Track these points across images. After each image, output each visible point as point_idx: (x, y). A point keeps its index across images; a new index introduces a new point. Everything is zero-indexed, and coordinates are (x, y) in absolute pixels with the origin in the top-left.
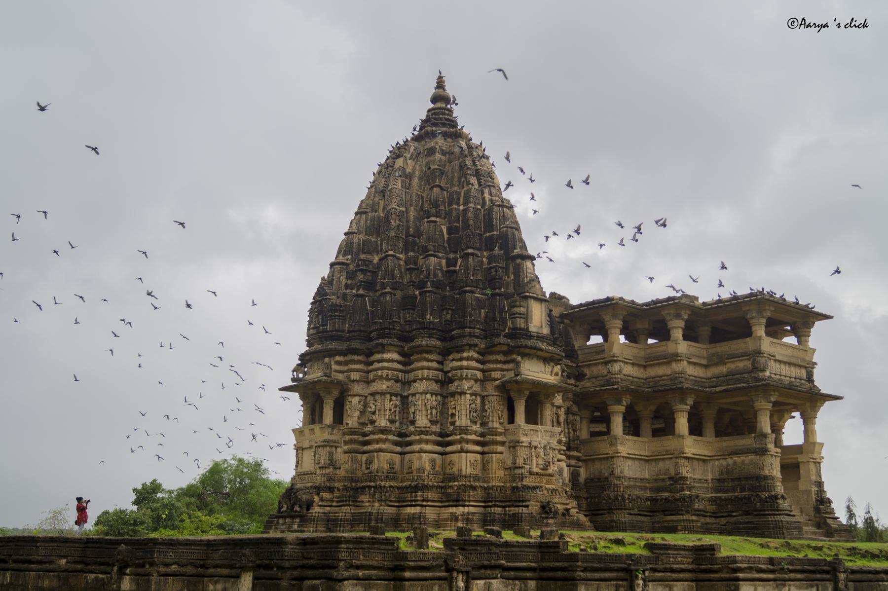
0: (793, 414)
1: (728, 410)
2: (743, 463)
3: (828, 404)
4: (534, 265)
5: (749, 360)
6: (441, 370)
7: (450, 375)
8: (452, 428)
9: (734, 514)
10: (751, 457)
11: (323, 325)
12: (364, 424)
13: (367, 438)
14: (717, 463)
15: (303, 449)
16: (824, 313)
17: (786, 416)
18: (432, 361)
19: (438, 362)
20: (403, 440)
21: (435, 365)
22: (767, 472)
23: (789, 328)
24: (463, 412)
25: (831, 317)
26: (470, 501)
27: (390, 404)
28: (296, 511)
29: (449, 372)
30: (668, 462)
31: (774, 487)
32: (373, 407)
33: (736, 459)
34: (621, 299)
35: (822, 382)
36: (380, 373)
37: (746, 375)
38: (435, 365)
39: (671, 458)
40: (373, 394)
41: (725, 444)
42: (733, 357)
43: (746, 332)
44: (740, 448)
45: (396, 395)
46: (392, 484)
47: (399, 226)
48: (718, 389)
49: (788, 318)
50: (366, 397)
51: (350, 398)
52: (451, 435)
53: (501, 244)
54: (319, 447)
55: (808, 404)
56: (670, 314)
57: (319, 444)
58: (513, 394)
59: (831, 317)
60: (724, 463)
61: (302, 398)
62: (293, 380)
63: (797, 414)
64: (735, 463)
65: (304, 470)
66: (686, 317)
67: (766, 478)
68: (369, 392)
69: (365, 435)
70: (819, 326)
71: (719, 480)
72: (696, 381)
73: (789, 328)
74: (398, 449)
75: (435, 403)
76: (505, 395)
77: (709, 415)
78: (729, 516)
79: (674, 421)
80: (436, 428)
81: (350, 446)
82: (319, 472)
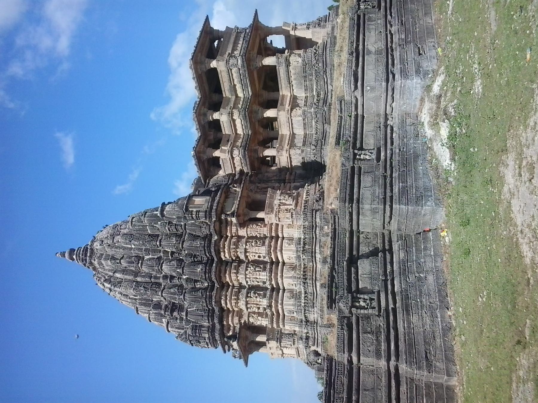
0: (269, 42)
1: (265, 82)
3: (260, 20)
4: (169, 203)
5: (231, 70)
6: (232, 263)
7: (234, 258)
9: (326, 81)
10: (291, 68)
11: (205, 339)
12: (267, 314)
13: (275, 313)
15: (283, 354)
16: (254, 15)
17: (270, 46)
19: (226, 266)
23: (216, 43)
24: (258, 252)
25: (256, 10)
26: (312, 248)
28: (321, 362)
29: (232, 259)
35: (246, 23)
37: (241, 72)
39: (292, 120)
40: (247, 308)
41: (283, 86)
42: (231, 80)
44: (285, 76)
47: (144, 287)
48: (315, 87)
49: (207, 43)
53: (155, 223)
54: (280, 345)
55: (259, 32)
56: (204, 119)
57: (278, 344)
58: (246, 219)
59: (256, 10)
61: (251, 352)
62: (240, 358)
63: (269, 39)
64: (295, 79)
65: (295, 353)
66: (206, 109)
68: (246, 310)
69: (273, 314)
70: (262, 20)
72: (202, 105)
73: (216, 43)
75: (252, 268)
76: (247, 223)
77: (267, 95)
78: (327, 83)
81: (280, 323)
82: (296, 345)
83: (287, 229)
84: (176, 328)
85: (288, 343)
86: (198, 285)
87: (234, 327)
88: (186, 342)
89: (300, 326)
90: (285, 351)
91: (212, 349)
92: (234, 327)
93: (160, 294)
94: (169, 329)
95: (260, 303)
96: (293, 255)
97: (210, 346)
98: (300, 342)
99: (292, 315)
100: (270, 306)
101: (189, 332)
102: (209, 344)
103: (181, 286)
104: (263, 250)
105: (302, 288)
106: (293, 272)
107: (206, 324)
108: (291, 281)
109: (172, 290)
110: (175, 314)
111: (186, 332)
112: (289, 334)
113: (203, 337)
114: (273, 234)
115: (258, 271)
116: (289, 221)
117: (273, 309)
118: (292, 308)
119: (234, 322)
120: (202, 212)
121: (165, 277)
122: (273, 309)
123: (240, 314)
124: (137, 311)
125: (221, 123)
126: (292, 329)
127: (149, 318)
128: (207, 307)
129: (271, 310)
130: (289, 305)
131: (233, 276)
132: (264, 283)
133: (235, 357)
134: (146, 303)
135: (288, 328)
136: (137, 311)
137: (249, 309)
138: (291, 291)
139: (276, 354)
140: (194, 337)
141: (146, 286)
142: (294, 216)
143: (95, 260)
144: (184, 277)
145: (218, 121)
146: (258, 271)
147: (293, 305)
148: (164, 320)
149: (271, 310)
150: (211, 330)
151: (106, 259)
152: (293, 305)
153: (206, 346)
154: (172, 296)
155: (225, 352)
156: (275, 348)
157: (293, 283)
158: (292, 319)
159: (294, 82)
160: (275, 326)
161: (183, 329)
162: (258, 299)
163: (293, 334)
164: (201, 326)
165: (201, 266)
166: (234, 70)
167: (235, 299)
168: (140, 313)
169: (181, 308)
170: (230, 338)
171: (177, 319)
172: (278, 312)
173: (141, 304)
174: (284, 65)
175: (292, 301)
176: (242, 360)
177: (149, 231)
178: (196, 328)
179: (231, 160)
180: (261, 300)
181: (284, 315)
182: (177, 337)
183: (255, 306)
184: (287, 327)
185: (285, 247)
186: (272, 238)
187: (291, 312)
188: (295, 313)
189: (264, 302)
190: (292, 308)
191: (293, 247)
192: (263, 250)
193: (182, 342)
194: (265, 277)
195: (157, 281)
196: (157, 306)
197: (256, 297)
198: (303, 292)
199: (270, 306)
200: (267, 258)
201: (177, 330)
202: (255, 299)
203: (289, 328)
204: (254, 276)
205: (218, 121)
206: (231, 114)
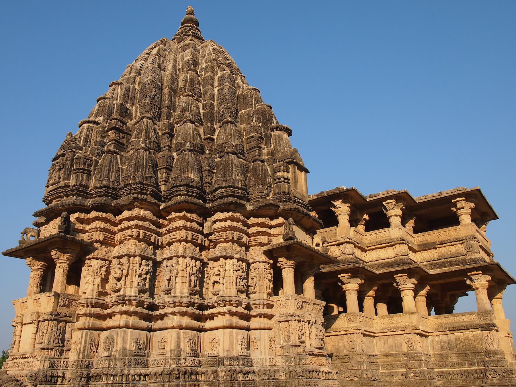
2: (467, 338)
5: (462, 244)
8: (215, 298)
10: (477, 333)
14: (437, 339)
18: (192, 221)
20: (150, 314)
21: (195, 225)
22: (495, 347)
27: (138, 269)
30: (398, 338)
31: (503, 359)
32: (119, 272)
33: (460, 334)
34: (322, 193)
36: (129, 232)
38: (195, 225)
43: (454, 220)
45: (147, 259)
46: (138, 371)
47: (155, 96)
50: (110, 262)
51: (87, 261)
52: (214, 307)
60: (445, 338)
62: (20, 242)
64: (457, 339)
67: (496, 353)
69: (104, 306)
71: (441, 355)
74: (145, 324)
79: (401, 300)
80: (196, 299)
83: (267, 339)
84: (87, 136)
85: (46, 337)
86: (162, 175)
87: (85, 232)
88: (63, 147)
89: (79, 364)
90: (29, 331)
91: (43, 192)
92: (85, 232)
93: (146, 115)
94: (86, 125)
95: (128, 283)
96: (221, 351)
97: (51, 188)
98: (47, 364)
99: (101, 346)
100: (123, 301)
101: (79, 154)
102: (55, 187)
103: (159, 149)
104: (229, 290)
105: (159, 369)
106: (188, 350)
107: (93, 182)
108: (171, 345)
109: (152, 133)
110: (111, 134)
111: (80, 149)
112: (63, 340)
113: (69, 175)
114: (254, 312)
115: (190, 281)
116: (281, 341)
117: (119, 308)
118: (118, 346)
119: (91, 232)
120: (289, 187)
121: (171, 127)
122: (119, 308)
123: (107, 243)
124: (115, 84)
125: (387, 229)
126: (73, 346)
127: (105, 98)
128: (125, 186)
129: (117, 303)
130: (124, 341)
131: (181, 234)
132: (167, 292)
133: (25, 233)
134: (128, 96)
135: (76, 338)
136: (115, 84)
137: (116, 264)
138: (148, 344)
139: (23, 312)
140: (72, 160)
141: (157, 97)
142: (294, 351)
143: (191, 40)
144: (175, 154)
145: (387, 225)
146: (190, 281)
147: (125, 349)
148: (101, 118)
149: (117, 303)
150: (82, 191)
151: (192, 54)
152: (125, 349)
153: (51, 182)
154: (144, 133)
155: (36, 215)
156: (37, 309)
157: (168, 348)
158: (94, 346)
159: (452, 336)
160: (82, 310)
161: (85, 145)
162: (137, 279)
163: (61, 344)
164: (89, 174)
165: (197, 179)
166: (461, 248)
167: (139, 236)
168: (112, 88)
169: (121, 146)
170: (67, 220)
171: (103, 137)
172: (110, 316)
173: (127, 89)
174: (482, 322)
175: (131, 346)
176: (18, 245)
177: (243, 111)
178: (87, 168)
179: (343, 240)
180: (135, 284)
181: (102, 330)
182: (71, 134)
183: (125, 272)
184: (77, 335)
185: (237, 335)
186: (249, 307)
187: (109, 345)
188: (106, 354)
189: (131, 291)
190: (118, 346)
191: (238, 350)
192: (229, 290)
193: (62, 142)
194: (178, 294)
195: (164, 116)
196: (125, 112)
197: (140, 276)
198: (148, 371)
199: (123, 301)
200: (215, 298)
201: (83, 135)
202: (138, 273)
203: (74, 338)
204: (180, 272)
205: (387, 225)
206: (402, 241)
